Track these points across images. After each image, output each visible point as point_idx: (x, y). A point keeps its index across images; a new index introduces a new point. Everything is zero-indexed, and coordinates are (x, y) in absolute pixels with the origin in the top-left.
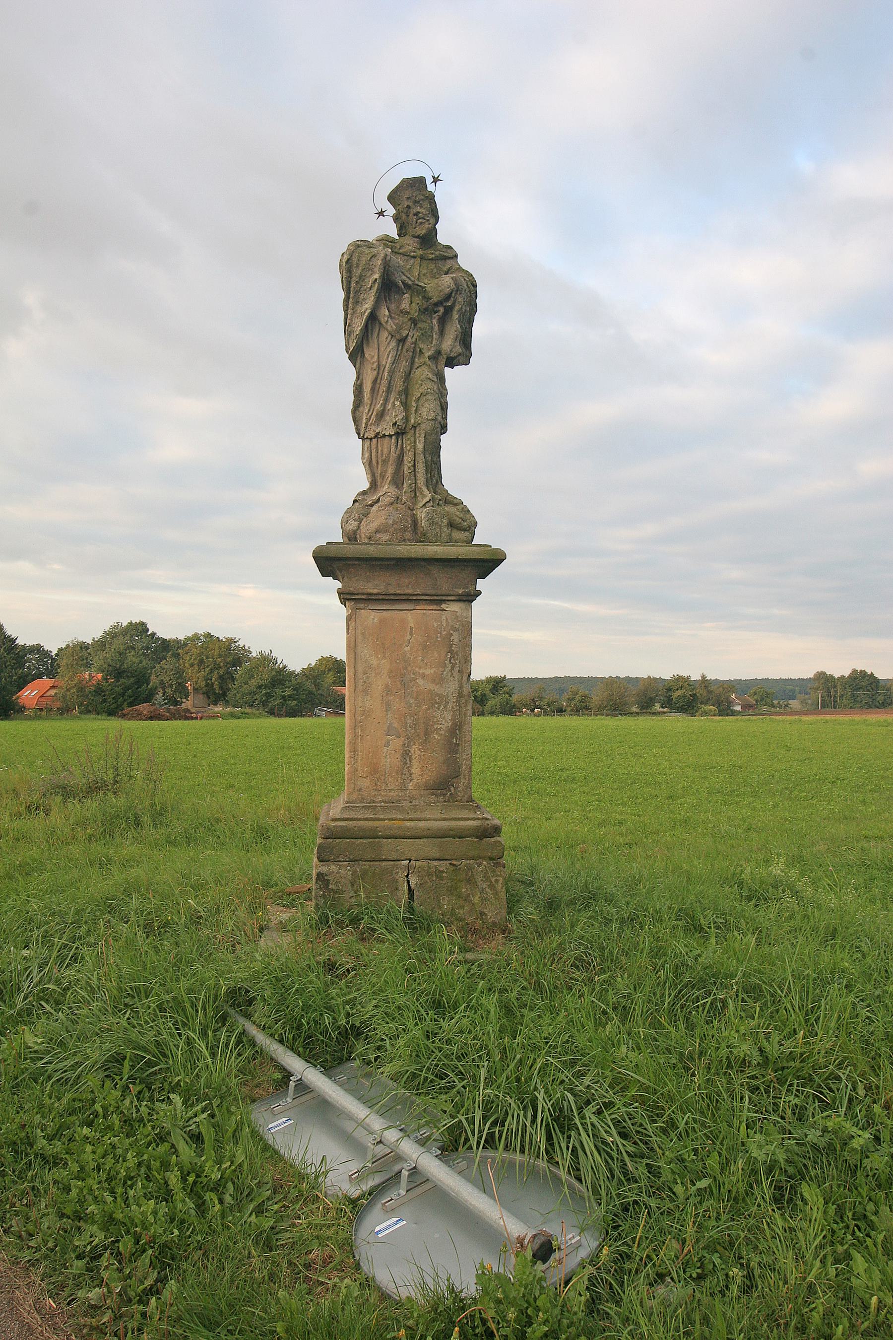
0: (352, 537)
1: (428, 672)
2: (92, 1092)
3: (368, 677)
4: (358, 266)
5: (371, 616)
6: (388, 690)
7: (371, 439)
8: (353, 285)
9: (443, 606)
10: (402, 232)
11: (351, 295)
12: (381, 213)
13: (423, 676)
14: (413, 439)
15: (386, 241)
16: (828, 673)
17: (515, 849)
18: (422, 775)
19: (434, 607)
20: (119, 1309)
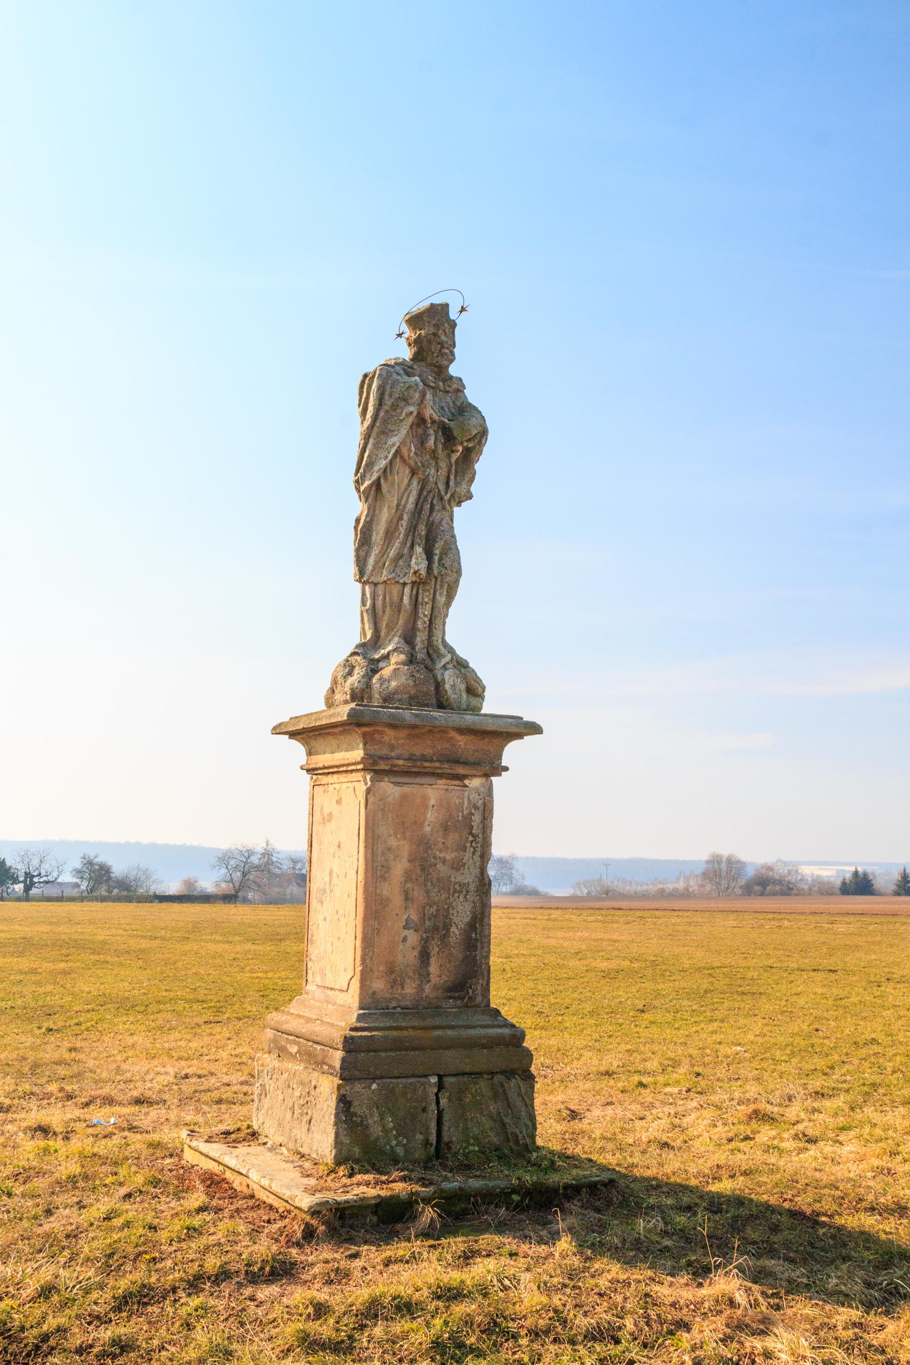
3: (386, 860)
5: (390, 789)
6: (408, 876)
7: (376, 584)
8: (382, 414)
9: (467, 782)
12: (400, 335)
13: (444, 861)
14: (432, 591)
16: (122, 842)
17: (338, 1049)
19: (457, 783)
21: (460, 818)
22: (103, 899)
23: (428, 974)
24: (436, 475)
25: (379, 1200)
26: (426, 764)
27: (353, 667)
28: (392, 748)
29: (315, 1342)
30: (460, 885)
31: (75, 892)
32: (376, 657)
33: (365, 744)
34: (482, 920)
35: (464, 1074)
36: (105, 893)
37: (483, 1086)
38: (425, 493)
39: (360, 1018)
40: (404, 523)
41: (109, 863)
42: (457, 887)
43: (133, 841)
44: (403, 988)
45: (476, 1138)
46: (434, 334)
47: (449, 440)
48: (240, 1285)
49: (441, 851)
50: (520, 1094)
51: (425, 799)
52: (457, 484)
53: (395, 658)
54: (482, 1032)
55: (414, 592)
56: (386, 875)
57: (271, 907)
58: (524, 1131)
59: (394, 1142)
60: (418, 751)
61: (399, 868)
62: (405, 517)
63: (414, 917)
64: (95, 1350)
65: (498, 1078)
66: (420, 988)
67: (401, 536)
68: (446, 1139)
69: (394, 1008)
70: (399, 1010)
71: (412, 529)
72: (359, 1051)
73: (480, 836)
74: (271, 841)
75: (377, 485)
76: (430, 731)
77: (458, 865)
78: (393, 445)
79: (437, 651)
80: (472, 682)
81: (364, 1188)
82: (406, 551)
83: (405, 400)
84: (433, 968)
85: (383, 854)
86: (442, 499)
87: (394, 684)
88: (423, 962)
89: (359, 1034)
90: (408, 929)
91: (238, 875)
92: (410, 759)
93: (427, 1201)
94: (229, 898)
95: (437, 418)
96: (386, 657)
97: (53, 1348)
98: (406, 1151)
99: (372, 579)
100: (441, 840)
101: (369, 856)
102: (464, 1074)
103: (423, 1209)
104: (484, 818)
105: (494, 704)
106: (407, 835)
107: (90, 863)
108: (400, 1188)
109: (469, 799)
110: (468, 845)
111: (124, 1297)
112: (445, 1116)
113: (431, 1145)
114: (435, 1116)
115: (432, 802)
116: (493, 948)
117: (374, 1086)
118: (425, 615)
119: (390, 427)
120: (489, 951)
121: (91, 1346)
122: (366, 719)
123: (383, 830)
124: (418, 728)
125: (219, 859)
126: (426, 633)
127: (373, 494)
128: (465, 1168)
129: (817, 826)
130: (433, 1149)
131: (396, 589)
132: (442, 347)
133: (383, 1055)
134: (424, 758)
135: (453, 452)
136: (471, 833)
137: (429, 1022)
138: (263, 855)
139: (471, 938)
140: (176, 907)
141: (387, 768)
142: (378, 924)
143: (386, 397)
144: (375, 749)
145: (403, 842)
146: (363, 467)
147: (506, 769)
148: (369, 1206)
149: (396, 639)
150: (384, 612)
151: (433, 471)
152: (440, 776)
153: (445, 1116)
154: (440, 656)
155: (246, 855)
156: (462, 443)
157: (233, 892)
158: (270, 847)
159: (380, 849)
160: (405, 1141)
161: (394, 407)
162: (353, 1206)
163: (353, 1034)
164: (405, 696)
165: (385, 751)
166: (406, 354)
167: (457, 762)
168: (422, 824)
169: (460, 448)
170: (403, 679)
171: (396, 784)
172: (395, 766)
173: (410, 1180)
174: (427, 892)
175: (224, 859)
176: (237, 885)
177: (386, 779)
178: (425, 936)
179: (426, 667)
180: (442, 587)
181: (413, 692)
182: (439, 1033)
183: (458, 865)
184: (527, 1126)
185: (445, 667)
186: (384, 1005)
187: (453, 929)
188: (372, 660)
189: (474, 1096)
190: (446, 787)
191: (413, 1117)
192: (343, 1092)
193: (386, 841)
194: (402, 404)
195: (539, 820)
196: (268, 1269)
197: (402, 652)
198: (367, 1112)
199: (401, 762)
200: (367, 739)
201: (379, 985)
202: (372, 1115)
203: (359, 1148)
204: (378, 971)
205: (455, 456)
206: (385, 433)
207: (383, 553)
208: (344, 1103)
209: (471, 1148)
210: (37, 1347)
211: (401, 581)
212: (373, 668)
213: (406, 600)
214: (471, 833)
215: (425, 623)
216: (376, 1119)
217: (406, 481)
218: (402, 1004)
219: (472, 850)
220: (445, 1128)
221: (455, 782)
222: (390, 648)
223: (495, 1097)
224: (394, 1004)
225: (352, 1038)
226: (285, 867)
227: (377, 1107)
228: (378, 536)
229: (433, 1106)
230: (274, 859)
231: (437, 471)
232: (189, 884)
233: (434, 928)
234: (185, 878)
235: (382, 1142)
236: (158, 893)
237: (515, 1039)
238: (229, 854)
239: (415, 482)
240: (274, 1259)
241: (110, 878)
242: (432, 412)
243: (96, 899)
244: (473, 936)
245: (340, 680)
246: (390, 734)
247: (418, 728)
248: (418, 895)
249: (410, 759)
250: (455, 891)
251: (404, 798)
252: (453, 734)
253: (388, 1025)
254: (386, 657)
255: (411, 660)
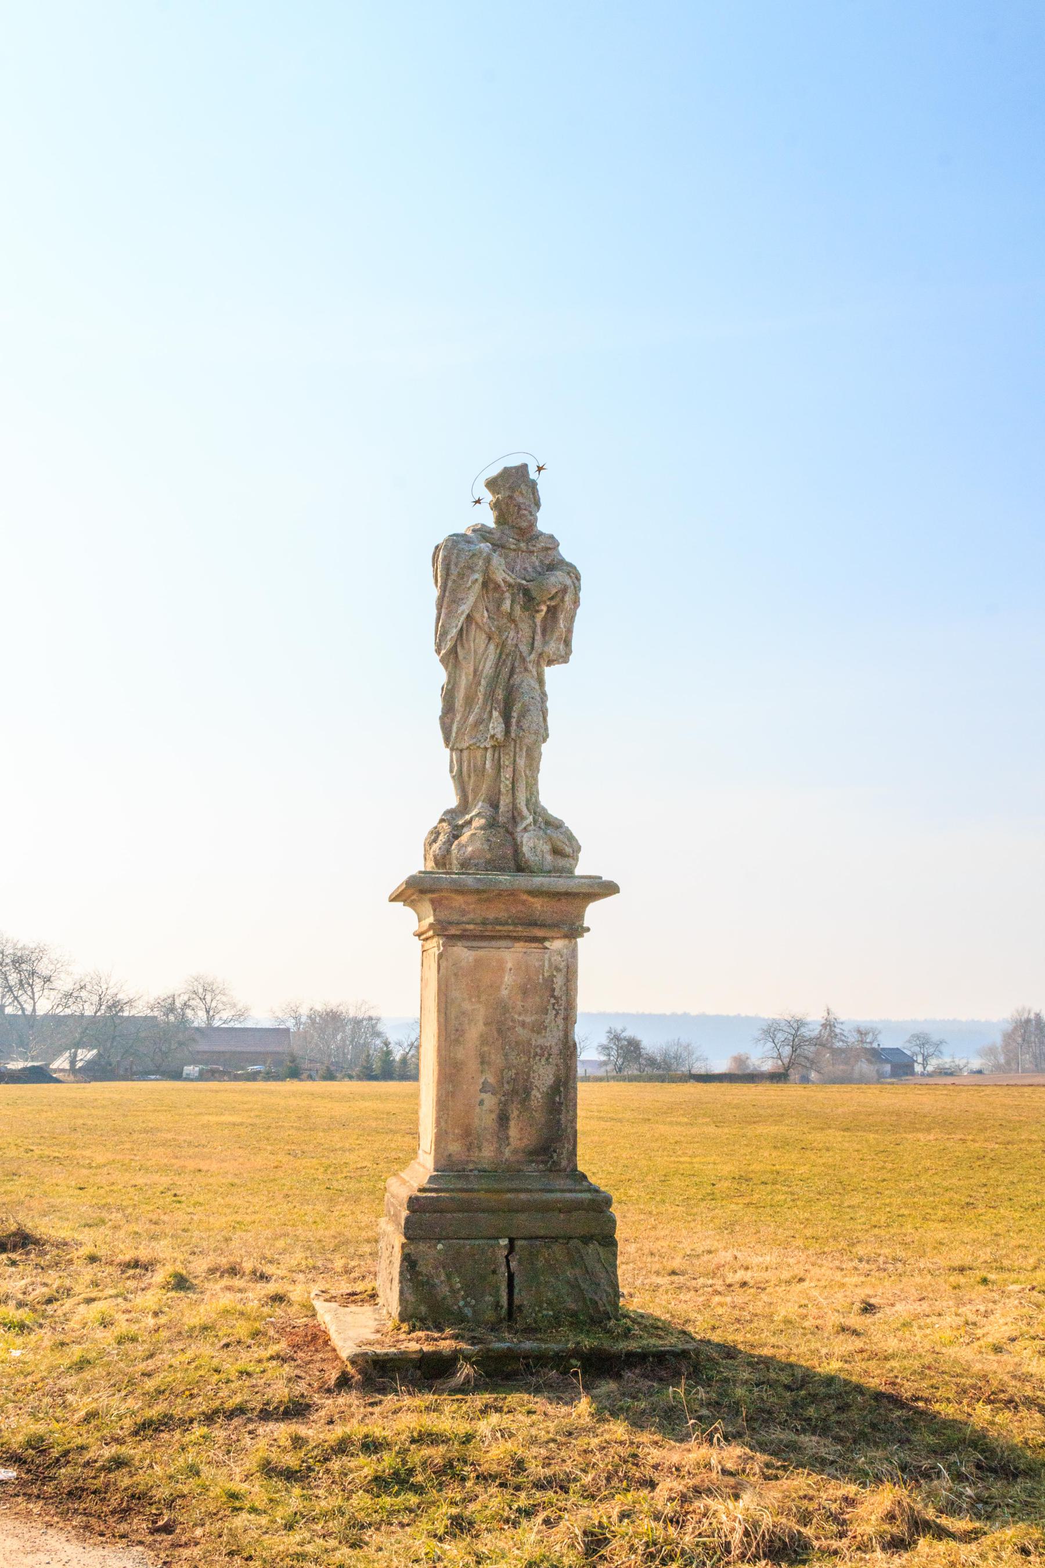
0: (442, 861)
1: (528, 1019)
2: (238, 1440)
4: (456, 565)
5: (463, 953)
6: (484, 1040)
7: (461, 751)
8: (450, 584)
9: (547, 944)
10: (501, 520)
11: (447, 594)
12: (478, 501)
13: (523, 1024)
14: (512, 754)
15: (482, 533)
18: (520, 1139)
19: (536, 945)
20: (584, 1323)
21: (541, 981)
22: (632, 1079)
23: (508, 1138)
24: (518, 636)
25: (420, 1355)
26: (498, 928)
27: (438, 834)
28: (464, 913)
29: (274, 1469)
30: (542, 1048)
31: (601, 1072)
32: (460, 822)
33: (435, 910)
34: (566, 1084)
35: (537, 1238)
36: (636, 1073)
37: (558, 1250)
38: (504, 657)
39: (432, 1179)
40: (482, 688)
41: (639, 1037)
42: (538, 1050)
43: (680, 1012)
44: (480, 1150)
45: (550, 1303)
46: (511, 497)
47: (529, 601)
48: (250, 1420)
49: (520, 1014)
50: (599, 1260)
51: (501, 963)
52: (545, 643)
53: (479, 822)
54: (558, 1195)
55: (496, 755)
56: (461, 1039)
57: (835, 1088)
58: (604, 1298)
59: (461, 1303)
60: (491, 916)
61: (474, 1032)
62: (483, 682)
63: (491, 1080)
64: (97, 1465)
65: (575, 1242)
66: (499, 1151)
67: (480, 701)
68: (517, 1302)
69: (471, 1171)
70: (476, 1173)
71: (490, 694)
72: (425, 1212)
73: (564, 998)
74: (833, 1010)
75: (454, 651)
76: (500, 895)
77: (539, 1028)
78: (462, 613)
79: (520, 813)
80: (559, 843)
81: (415, 1343)
82: (485, 716)
83: (471, 568)
84: (513, 1132)
85: (456, 1018)
86: (523, 660)
87: (470, 849)
88: (501, 1125)
89: (425, 1195)
90: (486, 1092)
91: (787, 1051)
92: (484, 924)
93: (467, 1358)
94: (778, 1077)
95: (511, 581)
96: (469, 822)
97: (69, 1462)
98: (474, 1312)
99: (457, 745)
100: (520, 1004)
101: (442, 1020)
102: (537, 1238)
103: (462, 1365)
104: (568, 980)
105: (585, 867)
106: (483, 998)
107: (617, 1038)
108: (446, 1345)
109: (550, 960)
110: (550, 1007)
111: (144, 1424)
112: (517, 1282)
113: (502, 1307)
114: (506, 1278)
115: (509, 965)
116: (579, 1112)
117: (440, 1246)
118: (507, 779)
119: (460, 596)
120: (575, 1116)
121: (96, 1461)
122: (427, 886)
123: (455, 994)
124: (504, 889)
125: (764, 1031)
126: (510, 795)
127: (451, 659)
128: (530, 1331)
129: (935, 985)
130: (504, 1312)
131: (479, 754)
132: (520, 509)
133: (449, 1215)
134: (498, 922)
135: (538, 611)
136: (553, 996)
137: (507, 1185)
138: (824, 1026)
139: (554, 1103)
140: (725, 1087)
141: (458, 933)
142: (454, 1086)
143: (453, 567)
144: (444, 915)
145: (477, 1006)
146: (441, 636)
147: (588, 930)
148: (411, 1360)
149: (480, 804)
150: (469, 777)
151: (512, 634)
152: (517, 939)
153: (517, 1282)
154: (523, 818)
155: (795, 1025)
156: (545, 602)
157: (782, 1071)
158: (831, 1017)
159: (453, 1012)
160: (473, 1301)
161: (461, 576)
162: (391, 1360)
163: (419, 1194)
164: (481, 861)
165: (455, 917)
166: (488, 518)
167: (534, 924)
168: (499, 988)
169: (544, 608)
170: (478, 844)
171: (470, 948)
172: (465, 930)
173: (463, 1337)
174: (506, 1055)
175: (770, 1031)
176: (786, 1061)
177: (459, 944)
178: (503, 1099)
179: (507, 831)
180: (521, 750)
181: (488, 856)
182: (509, 1196)
183: (539, 1028)
184: (608, 1295)
185: (525, 829)
186: (460, 1168)
187: (534, 1092)
188: (457, 826)
189: (547, 1261)
190: (524, 950)
191: (483, 1278)
192: (406, 1250)
193: (460, 1005)
194: (467, 572)
195: (620, 979)
196: (282, 1409)
197: (483, 817)
198: (433, 1271)
199: (471, 927)
200: (436, 904)
201: (455, 1147)
202: (438, 1276)
203: (423, 1307)
204: (454, 1134)
205: (539, 617)
206: (456, 601)
207: (465, 718)
208: (410, 1263)
209: (545, 1312)
210: (58, 1460)
211: (482, 746)
212: (456, 834)
213: (488, 765)
214: (553, 996)
215: (507, 786)
216: (443, 1278)
217: (483, 646)
218: (479, 1166)
219: (554, 1012)
220: (516, 1291)
221: (533, 945)
222: (473, 813)
223: (573, 1264)
224: (471, 1166)
225: (417, 1198)
226: (851, 1040)
227: (444, 1267)
228: (459, 703)
229: (503, 1269)
230: (838, 1031)
231: (518, 633)
232: (740, 1061)
233: (515, 1091)
234: (735, 1054)
235: (450, 1301)
236: (694, 1072)
237: (599, 1206)
238: (775, 1025)
239: (492, 647)
240: (290, 1400)
241: (640, 1055)
242: (504, 575)
243: (624, 1079)
244: (557, 1099)
245: (428, 848)
246: (459, 901)
247: (504, 889)
248: (497, 1059)
249: (484, 924)
250: (536, 1054)
251: (478, 963)
252: (525, 897)
253: (459, 1186)
254: (469, 822)
255: (492, 824)
